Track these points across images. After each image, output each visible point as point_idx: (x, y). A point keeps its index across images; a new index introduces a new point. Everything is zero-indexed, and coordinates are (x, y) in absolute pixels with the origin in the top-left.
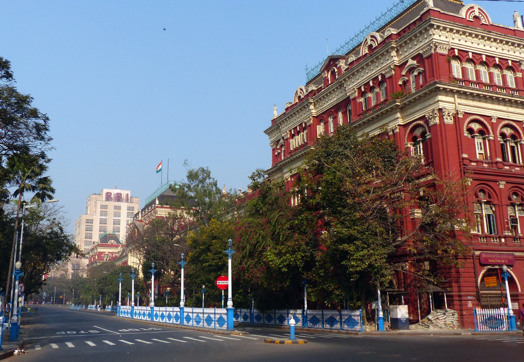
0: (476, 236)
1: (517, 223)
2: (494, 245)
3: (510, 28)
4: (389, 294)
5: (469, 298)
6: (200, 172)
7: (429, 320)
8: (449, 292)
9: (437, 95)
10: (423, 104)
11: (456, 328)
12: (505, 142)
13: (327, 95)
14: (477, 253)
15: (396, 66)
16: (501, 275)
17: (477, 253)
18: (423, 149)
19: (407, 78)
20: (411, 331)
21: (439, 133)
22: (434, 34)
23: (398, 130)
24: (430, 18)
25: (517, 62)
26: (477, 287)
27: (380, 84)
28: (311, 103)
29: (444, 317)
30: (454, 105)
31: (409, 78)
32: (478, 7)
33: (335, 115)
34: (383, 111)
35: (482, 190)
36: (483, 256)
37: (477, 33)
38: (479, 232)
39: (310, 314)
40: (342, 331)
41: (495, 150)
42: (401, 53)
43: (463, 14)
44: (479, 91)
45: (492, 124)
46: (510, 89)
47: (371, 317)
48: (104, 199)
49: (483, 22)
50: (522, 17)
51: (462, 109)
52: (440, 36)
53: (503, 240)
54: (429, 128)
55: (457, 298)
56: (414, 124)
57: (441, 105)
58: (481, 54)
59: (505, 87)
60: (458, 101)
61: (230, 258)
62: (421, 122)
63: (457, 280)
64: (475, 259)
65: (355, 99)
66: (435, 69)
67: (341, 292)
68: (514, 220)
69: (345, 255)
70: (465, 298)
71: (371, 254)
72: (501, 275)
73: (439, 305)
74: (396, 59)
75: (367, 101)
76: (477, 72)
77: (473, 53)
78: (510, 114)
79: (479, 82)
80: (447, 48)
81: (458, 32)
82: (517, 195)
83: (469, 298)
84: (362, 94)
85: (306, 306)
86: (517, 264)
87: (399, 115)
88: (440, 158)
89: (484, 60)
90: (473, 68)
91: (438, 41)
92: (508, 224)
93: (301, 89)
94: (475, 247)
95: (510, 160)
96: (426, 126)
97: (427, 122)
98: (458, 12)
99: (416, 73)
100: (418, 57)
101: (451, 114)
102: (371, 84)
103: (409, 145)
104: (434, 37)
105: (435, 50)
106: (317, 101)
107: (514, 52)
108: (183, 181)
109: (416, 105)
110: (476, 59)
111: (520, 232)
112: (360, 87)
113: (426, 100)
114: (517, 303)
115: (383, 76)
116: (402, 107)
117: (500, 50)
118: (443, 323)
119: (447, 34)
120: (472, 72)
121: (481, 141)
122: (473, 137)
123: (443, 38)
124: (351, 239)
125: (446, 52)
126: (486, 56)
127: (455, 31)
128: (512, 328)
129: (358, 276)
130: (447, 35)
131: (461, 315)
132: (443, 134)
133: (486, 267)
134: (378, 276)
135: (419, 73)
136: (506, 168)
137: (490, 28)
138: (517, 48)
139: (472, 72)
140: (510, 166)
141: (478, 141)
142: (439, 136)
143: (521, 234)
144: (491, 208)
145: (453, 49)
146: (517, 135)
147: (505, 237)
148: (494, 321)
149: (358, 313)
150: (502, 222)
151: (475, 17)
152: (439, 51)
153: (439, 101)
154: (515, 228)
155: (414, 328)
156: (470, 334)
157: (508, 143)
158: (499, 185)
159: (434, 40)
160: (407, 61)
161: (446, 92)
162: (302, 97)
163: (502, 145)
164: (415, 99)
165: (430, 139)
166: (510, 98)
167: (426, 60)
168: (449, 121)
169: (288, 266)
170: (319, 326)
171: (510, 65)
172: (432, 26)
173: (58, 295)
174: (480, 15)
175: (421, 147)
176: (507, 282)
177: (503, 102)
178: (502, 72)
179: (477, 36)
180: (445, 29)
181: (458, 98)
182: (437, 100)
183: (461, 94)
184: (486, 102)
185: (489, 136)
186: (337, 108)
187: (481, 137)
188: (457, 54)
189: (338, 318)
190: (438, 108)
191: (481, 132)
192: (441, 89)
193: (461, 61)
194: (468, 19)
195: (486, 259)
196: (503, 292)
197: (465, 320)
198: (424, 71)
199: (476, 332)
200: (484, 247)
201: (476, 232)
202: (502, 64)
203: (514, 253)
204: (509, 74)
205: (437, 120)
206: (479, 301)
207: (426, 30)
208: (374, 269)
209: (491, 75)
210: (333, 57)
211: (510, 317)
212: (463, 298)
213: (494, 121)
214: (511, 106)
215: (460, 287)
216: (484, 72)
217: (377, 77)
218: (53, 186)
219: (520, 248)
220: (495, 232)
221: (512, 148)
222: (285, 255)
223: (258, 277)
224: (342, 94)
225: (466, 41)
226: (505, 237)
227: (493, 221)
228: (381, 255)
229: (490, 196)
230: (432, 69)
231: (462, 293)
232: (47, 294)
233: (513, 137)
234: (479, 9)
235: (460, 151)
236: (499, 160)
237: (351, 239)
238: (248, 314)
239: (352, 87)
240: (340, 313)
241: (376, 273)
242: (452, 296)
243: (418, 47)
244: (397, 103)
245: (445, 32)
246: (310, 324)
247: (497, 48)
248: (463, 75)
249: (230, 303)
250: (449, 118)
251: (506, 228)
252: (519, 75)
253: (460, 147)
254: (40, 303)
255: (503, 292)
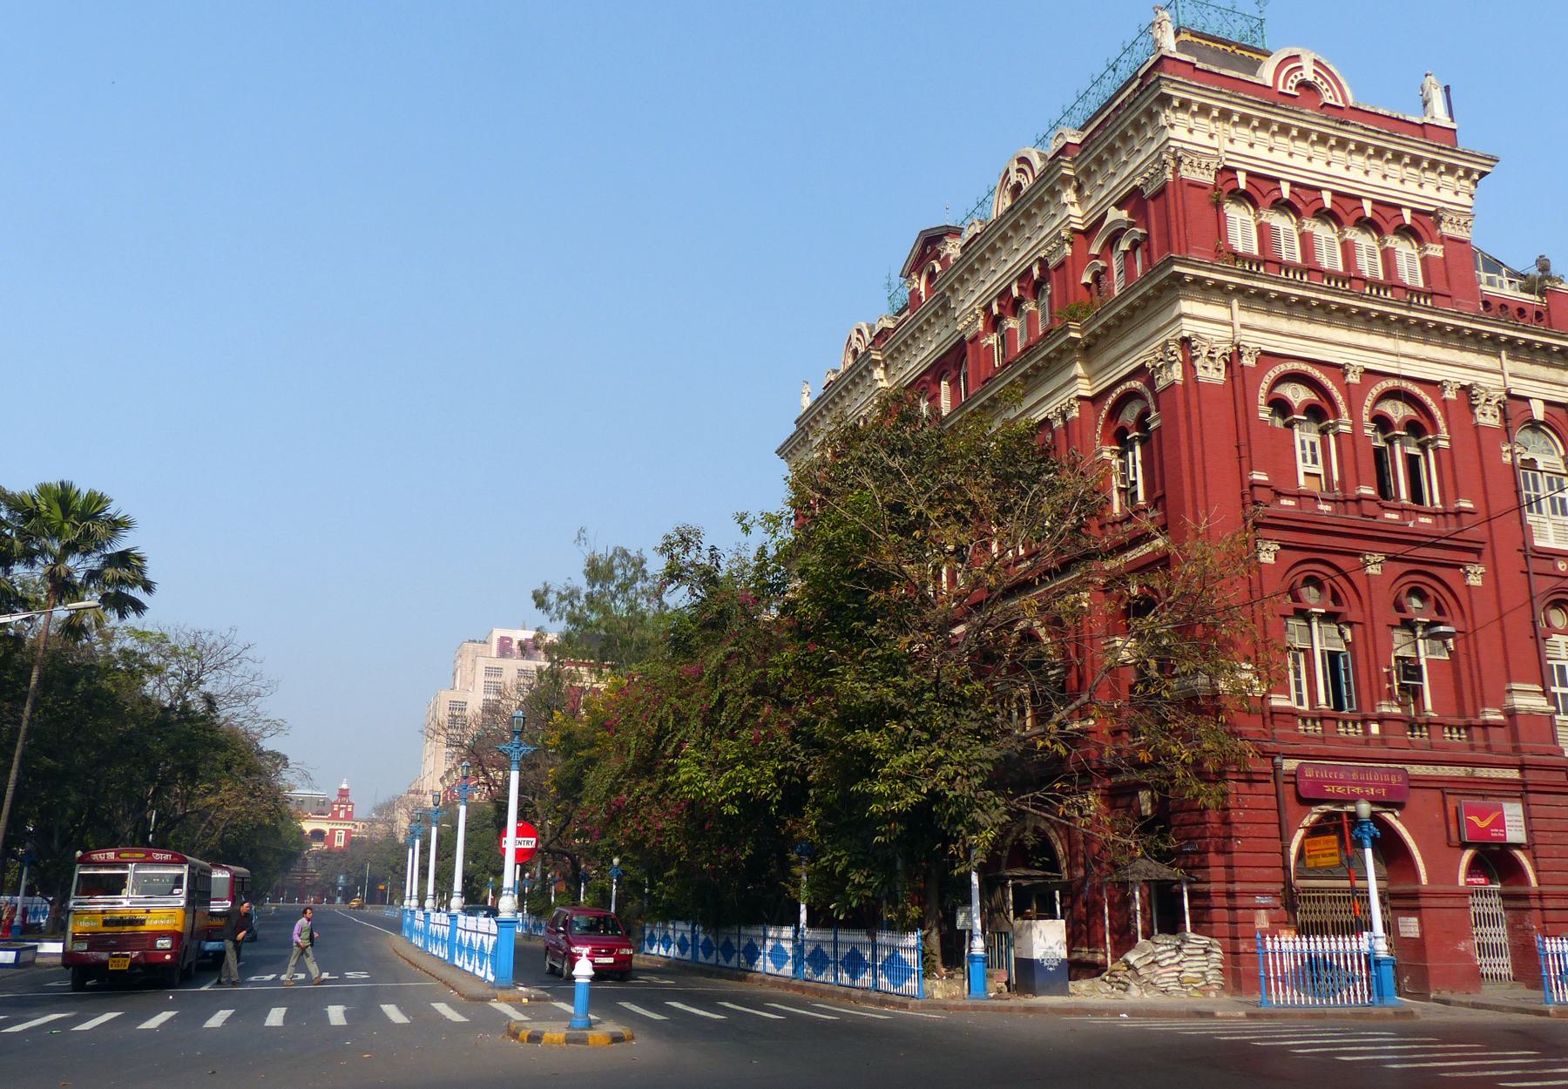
0: (1291, 714)
1: (1421, 679)
2: (1347, 741)
3: (1409, 118)
4: (1014, 886)
5: (1260, 900)
6: (616, 562)
7: (1130, 967)
8: (1199, 881)
9: (1177, 299)
10: (1144, 327)
11: (1213, 994)
12: (1390, 441)
13: (913, 336)
14: (1290, 765)
15: (1074, 231)
16: (1351, 830)
17: (1290, 765)
18: (1143, 463)
19: (1102, 263)
20: (1072, 999)
21: (1181, 412)
22: (1172, 126)
23: (1075, 413)
24: (1160, 78)
25: (1429, 214)
26: (1286, 868)
27: (1037, 288)
28: (876, 363)
29: (1177, 960)
30: (1229, 329)
31: (1109, 261)
32: (1313, 56)
33: (934, 388)
34: (1041, 366)
35: (1310, 581)
36: (1309, 773)
37: (1304, 125)
38: (1300, 702)
39: (810, 941)
40: (873, 994)
41: (1356, 463)
42: (1087, 193)
43: (1266, 75)
44: (1305, 288)
45: (1347, 389)
46: (1406, 288)
47: (952, 952)
48: (494, 654)
49: (1327, 98)
50: (1447, 89)
51: (1254, 341)
52: (1191, 131)
53: (1375, 729)
54: (1156, 396)
55: (1224, 902)
56: (1118, 391)
57: (1188, 328)
58: (1319, 189)
59: (1391, 283)
60: (1243, 317)
61: (515, 766)
62: (1136, 384)
63: (1224, 845)
64: (1281, 784)
65: (975, 338)
66: (1174, 225)
67: (868, 877)
68: (1411, 669)
69: (866, 764)
70: (1247, 901)
71: (939, 761)
72: (1351, 830)
73: (1170, 923)
74: (1076, 211)
75: (1007, 339)
76: (1306, 240)
77: (1293, 184)
78: (1403, 360)
79: (1310, 268)
80: (1212, 166)
81: (1245, 120)
82: (1423, 597)
83: (1260, 900)
84: (994, 323)
85: (803, 917)
86: (1416, 799)
87: (1079, 369)
88: (1181, 484)
89: (1328, 204)
90: (1293, 228)
91: (1186, 146)
92: (1391, 682)
93: (859, 331)
94: (1284, 748)
95: (1404, 494)
96: (1149, 395)
97: (1151, 383)
98: (1254, 66)
99: (1125, 245)
100: (1133, 200)
101: (1217, 354)
102: (1015, 292)
103: (1106, 455)
104: (1171, 133)
105: (1176, 170)
106: (891, 356)
107: (1421, 185)
108: (569, 584)
109: (1123, 337)
110: (1301, 202)
111: (1428, 706)
112: (990, 304)
113: (1148, 319)
114: (1415, 920)
115: (1043, 262)
116: (1088, 347)
117: (1375, 178)
118: (1171, 979)
119: (1212, 126)
120: (1290, 240)
121: (1315, 437)
122: (1289, 426)
123: (1200, 137)
124: (876, 716)
125: (1208, 178)
126: (1335, 193)
127: (1236, 118)
128: (1381, 995)
129: (900, 828)
130: (1212, 127)
131: (1233, 954)
132: (1194, 411)
133: (1314, 809)
134: (960, 827)
135: (1135, 245)
136: (1388, 515)
137: (1341, 114)
138: (1429, 175)
139: (1290, 240)
140: (1402, 510)
141: (1305, 436)
142: (1182, 418)
143: (1434, 710)
144: (1341, 634)
145: (1233, 170)
146: (1425, 422)
147: (1381, 720)
148: (1322, 971)
149: (912, 940)
150: (1373, 675)
151: (1304, 85)
152: (1186, 173)
153: (1181, 316)
154: (1417, 693)
155: (1086, 992)
156: (1241, 1014)
157: (1397, 446)
158: (1365, 566)
159: (1171, 143)
160: (1105, 215)
161: (1201, 289)
162: (861, 350)
163: (1379, 452)
164: (1118, 317)
165: (1158, 429)
166: (1404, 312)
167: (1151, 203)
168: (1212, 374)
169: (743, 799)
170: (827, 977)
171: (1408, 221)
172: (1165, 100)
173: (374, 882)
174: (1319, 80)
175: (1139, 458)
176: (1369, 852)
177: (1383, 323)
178: (1382, 242)
179: (1304, 135)
180: (1204, 110)
181: (1241, 308)
182: (1176, 313)
183: (1250, 297)
184: (1329, 324)
185: (1337, 424)
186: (940, 369)
187: (1314, 427)
188: (1243, 185)
189: (867, 955)
190: (1178, 337)
191: (1315, 413)
192: (1188, 279)
193: (1256, 206)
194: (1281, 89)
195: (1318, 784)
196: (1359, 884)
197: (1241, 971)
198: (1146, 237)
199: (1262, 1009)
200: (1312, 748)
201: (1293, 703)
202: (1383, 220)
203: (1407, 767)
204: (1405, 251)
205: (1177, 373)
206: (1295, 911)
207: (1152, 116)
208: (948, 808)
209: (1348, 249)
210: (931, 234)
211: (1378, 962)
212: (1239, 902)
213: (1353, 379)
214: (1407, 339)
215: (1231, 867)
216: (1329, 240)
217: (1030, 269)
218: (150, 575)
219: (1428, 754)
220: (1350, 705)
221: (1412, 462)
222: (733, 767)
223: (661, 832)
224: (950, 331)
225: (1271, 149)
226: (1381, 720)
227: (1347, 671)
228: (971, 763)
229: (1336, 598)
230: (1167, 230)
231: (1238, 887)
232: (347, 879)
233: (1414, 428)
234: (1316, 62)
235: (1244, 461)
236: (1368, 491)
237: (876, 716)
238: (688, 936)
239: (969, 305)
240: (874, 941)
241: (954, 820)
242: (1206, 895)
243: (1131, 169)
244: (1072, 334)
245: (1206, 121)
246: (808, 970)
247: (1367, 172)
248: (1262, 248)
249: (507, 904)
250: (1211, 365)
251: (1385, 693)
252: (1436, 251)
253: (1244, 451)
254: (332, 900)
255: (1359, 884)
